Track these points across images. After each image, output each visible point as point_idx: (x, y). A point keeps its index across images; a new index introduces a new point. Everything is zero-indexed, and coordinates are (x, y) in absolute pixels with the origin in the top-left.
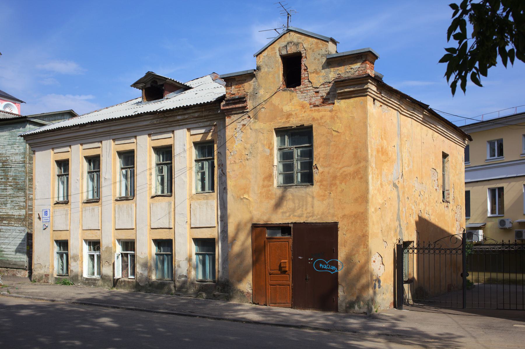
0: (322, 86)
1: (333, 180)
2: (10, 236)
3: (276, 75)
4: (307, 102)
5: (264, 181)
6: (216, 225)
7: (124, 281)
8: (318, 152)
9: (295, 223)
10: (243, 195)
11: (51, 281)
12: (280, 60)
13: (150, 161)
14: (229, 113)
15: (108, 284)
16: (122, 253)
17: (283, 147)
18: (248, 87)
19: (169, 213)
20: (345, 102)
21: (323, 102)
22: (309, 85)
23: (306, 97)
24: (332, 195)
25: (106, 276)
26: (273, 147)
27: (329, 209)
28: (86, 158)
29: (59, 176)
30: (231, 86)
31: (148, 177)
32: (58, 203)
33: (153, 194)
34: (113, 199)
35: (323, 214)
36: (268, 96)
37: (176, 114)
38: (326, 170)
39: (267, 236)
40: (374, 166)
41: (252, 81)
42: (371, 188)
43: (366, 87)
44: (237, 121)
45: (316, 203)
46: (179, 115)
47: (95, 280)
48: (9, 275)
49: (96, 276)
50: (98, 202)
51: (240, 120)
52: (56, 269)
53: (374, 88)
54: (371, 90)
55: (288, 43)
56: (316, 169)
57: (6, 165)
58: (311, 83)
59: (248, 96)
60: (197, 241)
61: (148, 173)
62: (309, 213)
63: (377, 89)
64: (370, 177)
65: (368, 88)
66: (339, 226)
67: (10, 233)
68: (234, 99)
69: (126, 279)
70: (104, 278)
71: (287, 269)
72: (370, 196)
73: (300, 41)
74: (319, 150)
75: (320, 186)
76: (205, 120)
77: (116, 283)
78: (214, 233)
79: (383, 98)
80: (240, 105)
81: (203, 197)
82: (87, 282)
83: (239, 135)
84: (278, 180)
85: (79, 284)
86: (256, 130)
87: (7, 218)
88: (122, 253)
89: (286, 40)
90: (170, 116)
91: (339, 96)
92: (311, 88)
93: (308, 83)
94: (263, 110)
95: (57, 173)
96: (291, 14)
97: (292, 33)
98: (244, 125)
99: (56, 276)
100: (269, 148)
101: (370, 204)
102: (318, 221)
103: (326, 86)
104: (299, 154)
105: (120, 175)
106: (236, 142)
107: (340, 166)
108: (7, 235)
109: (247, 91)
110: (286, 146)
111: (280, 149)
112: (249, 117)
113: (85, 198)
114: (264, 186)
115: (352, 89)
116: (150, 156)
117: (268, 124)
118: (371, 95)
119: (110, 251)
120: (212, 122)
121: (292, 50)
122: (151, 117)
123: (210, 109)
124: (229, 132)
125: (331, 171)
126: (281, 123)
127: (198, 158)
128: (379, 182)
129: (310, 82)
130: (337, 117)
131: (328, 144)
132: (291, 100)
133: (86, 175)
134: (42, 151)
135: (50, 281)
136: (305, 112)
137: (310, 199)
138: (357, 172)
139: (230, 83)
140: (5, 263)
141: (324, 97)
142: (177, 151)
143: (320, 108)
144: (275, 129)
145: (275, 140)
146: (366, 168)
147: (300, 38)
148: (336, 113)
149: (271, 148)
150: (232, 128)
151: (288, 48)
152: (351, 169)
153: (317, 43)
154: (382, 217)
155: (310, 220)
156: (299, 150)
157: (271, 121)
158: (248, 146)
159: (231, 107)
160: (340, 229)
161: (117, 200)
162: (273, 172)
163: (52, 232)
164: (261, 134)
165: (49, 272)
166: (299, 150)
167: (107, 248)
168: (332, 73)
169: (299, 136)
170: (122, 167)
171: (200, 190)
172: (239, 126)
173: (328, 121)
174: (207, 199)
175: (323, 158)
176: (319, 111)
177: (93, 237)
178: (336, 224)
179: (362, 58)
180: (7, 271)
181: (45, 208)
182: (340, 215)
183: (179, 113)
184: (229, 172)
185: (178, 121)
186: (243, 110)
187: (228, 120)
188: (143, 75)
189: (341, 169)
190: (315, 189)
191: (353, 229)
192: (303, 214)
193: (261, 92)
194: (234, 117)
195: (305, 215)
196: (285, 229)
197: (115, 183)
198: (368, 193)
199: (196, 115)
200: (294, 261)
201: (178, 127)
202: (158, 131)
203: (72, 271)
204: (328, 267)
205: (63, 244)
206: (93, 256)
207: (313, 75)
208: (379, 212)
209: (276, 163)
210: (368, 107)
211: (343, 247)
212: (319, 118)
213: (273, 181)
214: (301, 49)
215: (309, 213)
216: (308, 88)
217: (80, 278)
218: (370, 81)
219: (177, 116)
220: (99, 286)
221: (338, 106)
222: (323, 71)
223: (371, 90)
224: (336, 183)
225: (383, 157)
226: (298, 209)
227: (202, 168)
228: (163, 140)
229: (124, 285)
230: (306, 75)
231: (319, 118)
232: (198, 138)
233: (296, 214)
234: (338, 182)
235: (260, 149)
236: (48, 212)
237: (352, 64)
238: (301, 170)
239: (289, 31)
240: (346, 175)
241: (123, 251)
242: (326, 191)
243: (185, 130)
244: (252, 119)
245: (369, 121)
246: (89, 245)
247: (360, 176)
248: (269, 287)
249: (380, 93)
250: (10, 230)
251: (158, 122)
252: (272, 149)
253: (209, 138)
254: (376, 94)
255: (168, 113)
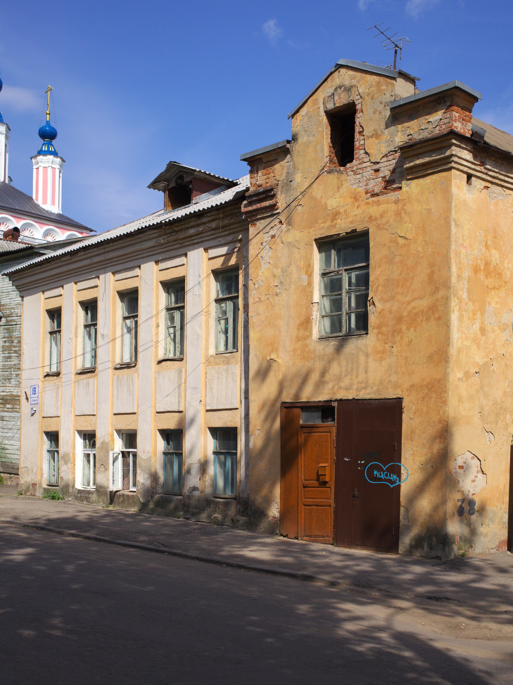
0: (385, 159)
1: (397, 324)
2: (14, 427)
3: (319, 147)
4: (361, 190)
5: (298, 329)
6: (237, 405)
7: (123, 495)
8: (376, 275)
9: (341, 400)
10: (270, 355)
11: (39, 493)
12: (325, 120)
13: (157, 304)
14: (253, 217)
15: (103, 499)
16: (123, 452)
17: (327, 271)
18: (280, 170)
19: (179, 386)
20: (417, 185)
21: (385, 188)
22: (366, 160)
23: (361, 180)
24: (395, 350)
25: (101, 488)
26: (312, 272)
27: (390, 375)
28: (82, 303)
29: (51, 333)
30: (257, 171)
31: (154, 330)
32: (47, 375)
33: (161, 357)
34: (110, 365)
35: (381, 383)
36: (307, 184)
37: (188, 226)
38: (388, 305)
39: (301, 422)
40: (465, 296)
41: (285, 161)
42: (455, 335)
43: (448, 153)
44: (264, 231)
45: (372, 364)
46: (192, 227)
47: (89, 492)
48: (12, 484)
49: (92, 487)
50: (93, 372)
51: (268, 228)
52: (45, 476)
53: (467, 155)
54: (460, 158)
55: (336, 90)
56: (372, 306)
57: (11, 321)
58: (369, 155)
59: (280, 187)
60: (215, 431)
61: (153, 322)
62: (362, 383)
63: (475, 157)
64: (454, 317)
65: (452, 155)
66: (404, 404)
67: (14, 422)
68: (257, 194)
69: (126, 492)
70: (100, 490)
71: (327, 479)
72: (453, 351)
73: (354, 82)
74: (378, 271)
75: (377, 335)
76: (227, 233)
77: (113, 496)
78: (234, 420)
79: (491, 173)
80: (267, 203)
81: (222, 360)
82: (79, 495)
83: (267, 254)
84: (319, 327)
85: (70, 499)
86: (290, 243)
87: (11, 400)
88: (123, 452)
89: (334, 84)
90: (181, 230)
91: (408, 174)
92: (368, 164)
93: (364, 156)
94: (299, 208)
95: (49, 329)
96: (401, 46)
97: (343, 71)
98: (273, 237)
99: (45, 486)
100: (307, 272)
101: (451, 365)
102: (373, 396)
103: (390, 158)
104: (353, 280)
105: (122, 329)
106: (263, 265)
107: (407, 299)
108: (11, 424)
109: (278, 178)
110: (332, 269)
111: (324, 275)
112: (281, 222)
113: (80, 367)
114: (298, 339)
115: (427, 159)
116: (157, 297)
117: (306, 231)
118: (461, 168)
119: (107, 447)
120: (236, 235)
121: (341, 100)
122: (155, 233)
123: (232, 214)
124: (253, 249)
125: (394, 308)
126: (325, 230)
127: (221, 296)
128: (477, 326)
129: (366, 153)
130: (405, 213)
131: (390, 261)
132: (338, 188)
133: (81, 330)
134: (31, 295)
135: (37, 494)
136: (358, 207)
137: (362, 358)
138: (433, 308)
139: (255, 168)
140: (8, 467)
141: (387, 178)
142: (189, 285)
143: (381, 198)
144: (316, 240)
145: (317, 258)
146: (447, 300)
147: (354, 78)
148: (404, 205)
149: (309, 273)
150: (257, 244)
151: (336, 98)
152: (423, 304)
153: (378, 83)
154: (482, 388)
155: (363, 395)
156: (353, 275)
157: (310, 227)
158: (278, 272)
159: (254, 207)
160: (405, 410)
161: (116, 369)
162: (311, 315)
163: (41, 418)
164: (296, 250)
165: (36, 480)
166: (353, 275)
167: (103, 443)
168: (400, 134)
169: (350, 248)
170: (127, 315)
171: (222, 348)
172: (266, 238)
173: (391, 220)
174: (228, 363)
175: (384, 286)
176: (378, 203)
177: (87, 427)
178: (399, 401)
179: (445, 102)
180: (10, 478)
181: (33, 382)
182: (406, 386)
183: (192, 224)
184: (251, 317)
185: (191, 236)
186: (271, 211)
187: (252, 230)
188: (163, 168)
189: (409, 303)
190: (369, 341)
191: (425, 410)
192: (352, 384)
193: (298, 178)
194: (261, 224)
195: (355, 387)
196: (326, 410)
197: (114, 340)
198: (449, 345)
199: (214, 225)
200: (339, 463)
201: (192, 247)
202: (167, 255)
203: (62, 478)
204: (386, 475)
205: (53, 437)
206: (88, 455)
207: (371, 140)
208: (476, 379)
209: (316, 297)
210: (454, 190)
211: (410, 442)
212: (378, 216)
213: (311, 328)
214: (354, 97)
215: (362, 383)
216: (364, 165)
217: (71, 490)
218: (454, 141)
219: (188, 228)
220: (93, 502)
221: (407, 192)
222: (386, 131)
223: (460, 158)
224: (401, 329)
225: (490, 280)
226: (346, 376)
227: (225, 313)
228: (172, 269)
229: (123, 502)
230: (362, 142)
231: (378, 216)
232: (218, 263)
233: (342, 384)
234: (404, 327)
235: (295, 276)
236: (37, 389)
237: (430, 113)
238: (357, 308)
239: (339, 67)
240: (416, 314)
241: (126, 448)
242: (386, 343)
243: (201, 250)
244: (284, 226)
245: (454, 215)
246: (85, 439)
247: (437, 316)
248: (302, 508)
249: (483, 164)
250: (14, 417)
251: (166, 241)
252: (310, 275)
253: (233, 261)
254: (473, 166)
255: (177, 224)
